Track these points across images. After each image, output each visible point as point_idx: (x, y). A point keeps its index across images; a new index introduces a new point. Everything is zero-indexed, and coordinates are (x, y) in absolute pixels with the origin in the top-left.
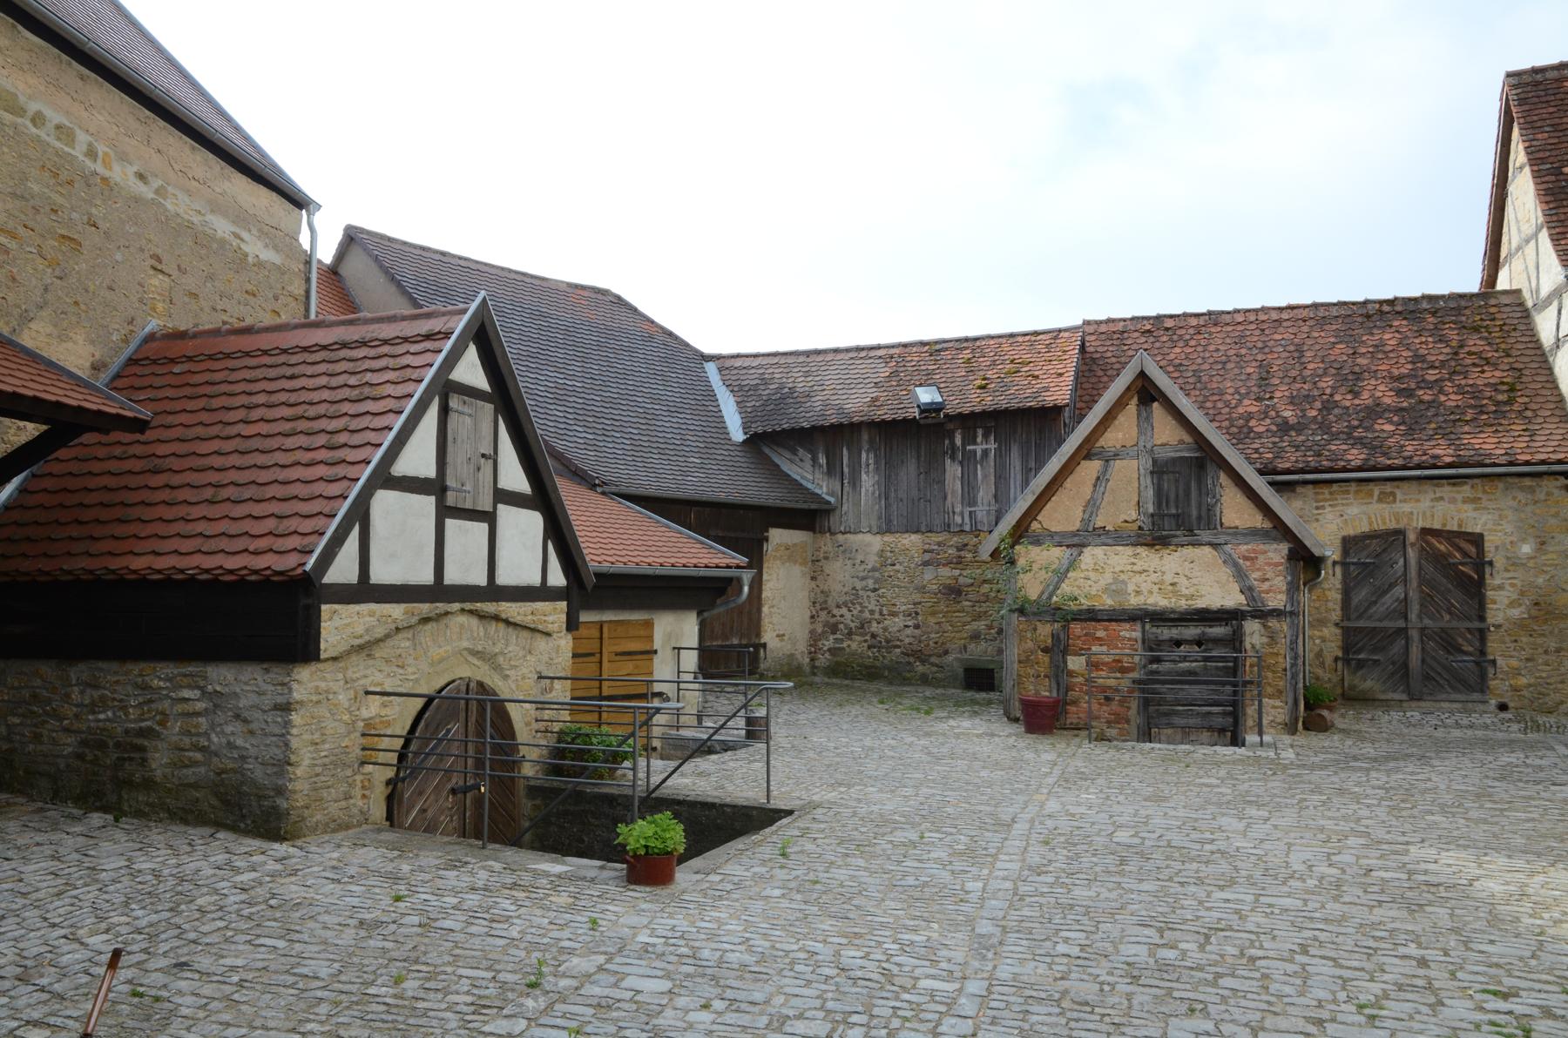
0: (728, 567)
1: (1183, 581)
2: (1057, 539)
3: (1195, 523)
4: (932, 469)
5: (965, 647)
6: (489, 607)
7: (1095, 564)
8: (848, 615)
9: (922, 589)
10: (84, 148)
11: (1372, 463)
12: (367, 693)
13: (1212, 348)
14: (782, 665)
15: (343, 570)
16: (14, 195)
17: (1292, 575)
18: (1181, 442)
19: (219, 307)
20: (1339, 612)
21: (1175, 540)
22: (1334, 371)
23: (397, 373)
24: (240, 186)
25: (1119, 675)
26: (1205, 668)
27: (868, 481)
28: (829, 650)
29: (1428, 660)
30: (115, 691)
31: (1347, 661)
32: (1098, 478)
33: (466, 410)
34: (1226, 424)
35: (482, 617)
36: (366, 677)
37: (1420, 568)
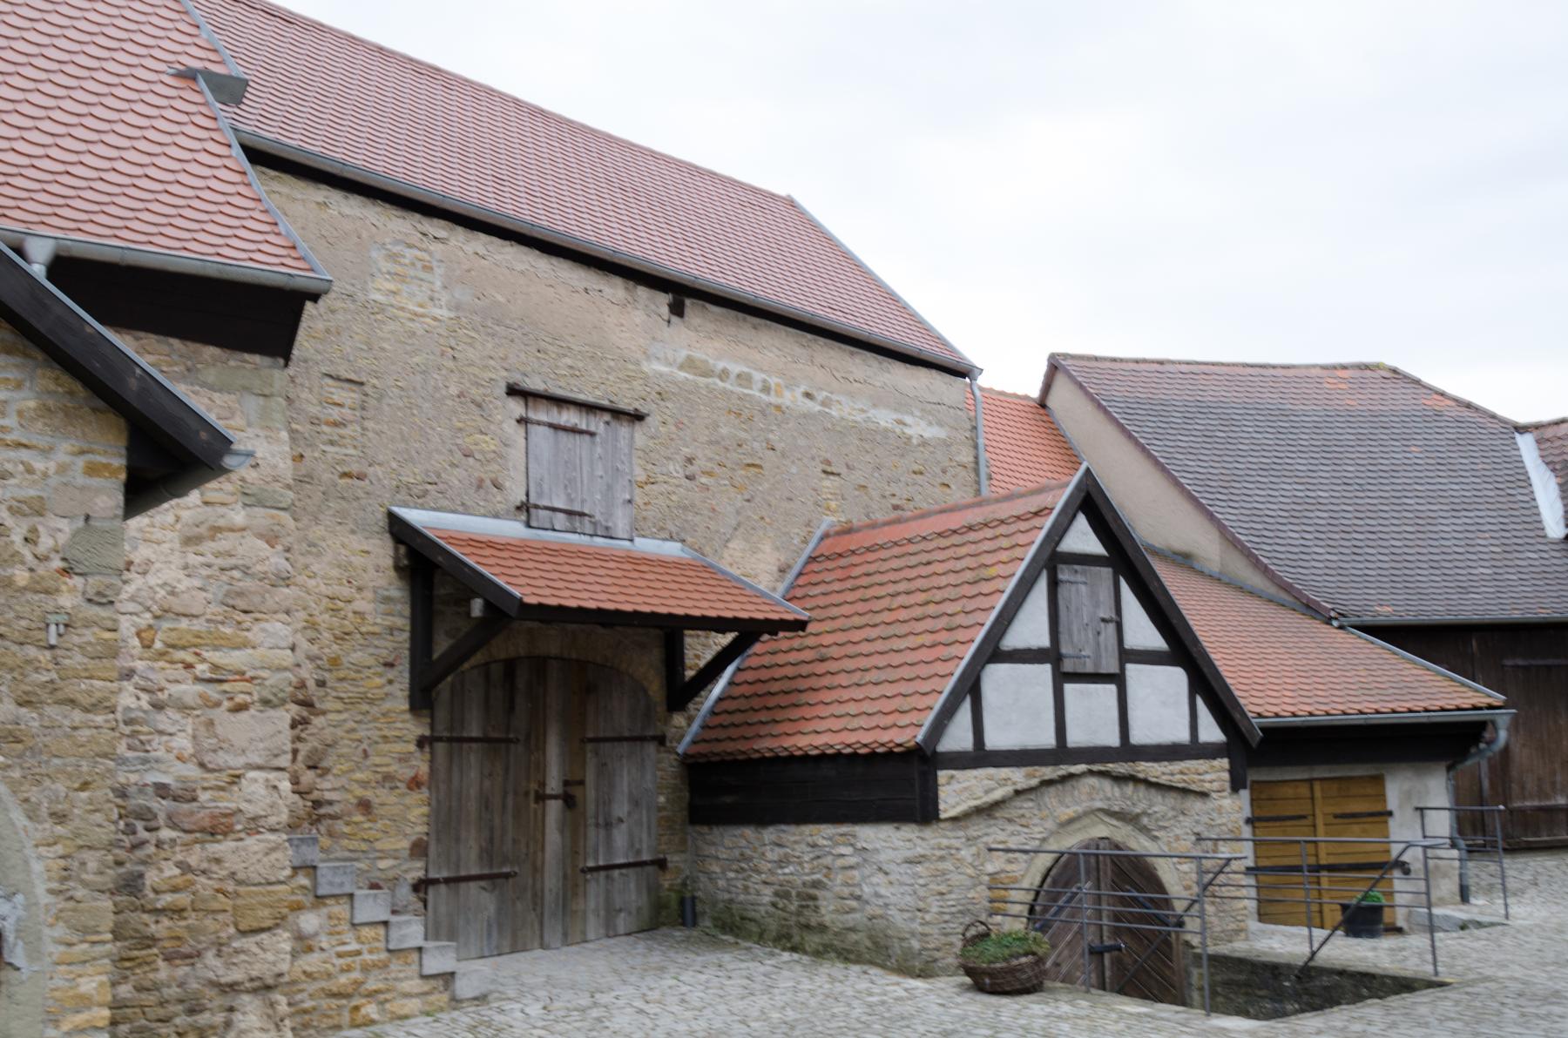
0: (1475, 708)
10: (760, 385)
12: (990, 850)
15: (958, 737)
16: (710, 443)
19: (887, 493)
24: (901, 375)
30: (793, 850)
33: (1079, 578)
35: (1119, 779)
36: (987, 834)
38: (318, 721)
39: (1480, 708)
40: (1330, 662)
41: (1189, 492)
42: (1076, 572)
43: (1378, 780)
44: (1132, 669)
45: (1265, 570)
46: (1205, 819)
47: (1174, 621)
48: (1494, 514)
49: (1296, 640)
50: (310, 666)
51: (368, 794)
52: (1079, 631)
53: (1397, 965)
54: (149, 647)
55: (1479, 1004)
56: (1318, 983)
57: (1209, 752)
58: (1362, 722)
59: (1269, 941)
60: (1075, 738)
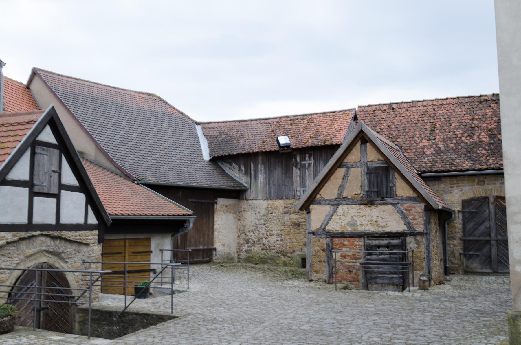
0: (184, 215)
1: (380, 220)
2: (328, 202)
3: (385, 194)
4: (288, 172)
5: (302, 249)
6: (55, 233)
7: (344, 213)
8: (253, 235)
9: (284, 224)
11: (473, 167)
13: (412, 117)
14: (224, 258)
17: (427, 217)
18: (379, 160)
20: (461, 233)
21: (377, 202)
22: (463, 127)
23: (13, 138)
25: (354, 261)
26: (390, 257)
27: (261, 177)
28: (246, 251)
29: (500, 254)
31: (465, 255)
32: (344, 176)
33: (45, 152)
34: (414, 150)
35: (54, 238)
37: (496, 213)
39: (185, 215)
40: (135, 196)
41: (85, 129)
42: (44, 149)
43: (148, 240)
44: (64, 194)
45: (112, 161)
46: (87, 254)
47: (83, 175)
48: (188, 150)
49: (123, 187)
52: (43, 175)
53: (156, 310)
54: (423, 268)
55: (191, 325)
56: (127, 318)
57: (91, 228)
58: (167, 219)
59: (107, 301)
60: (37, 220)
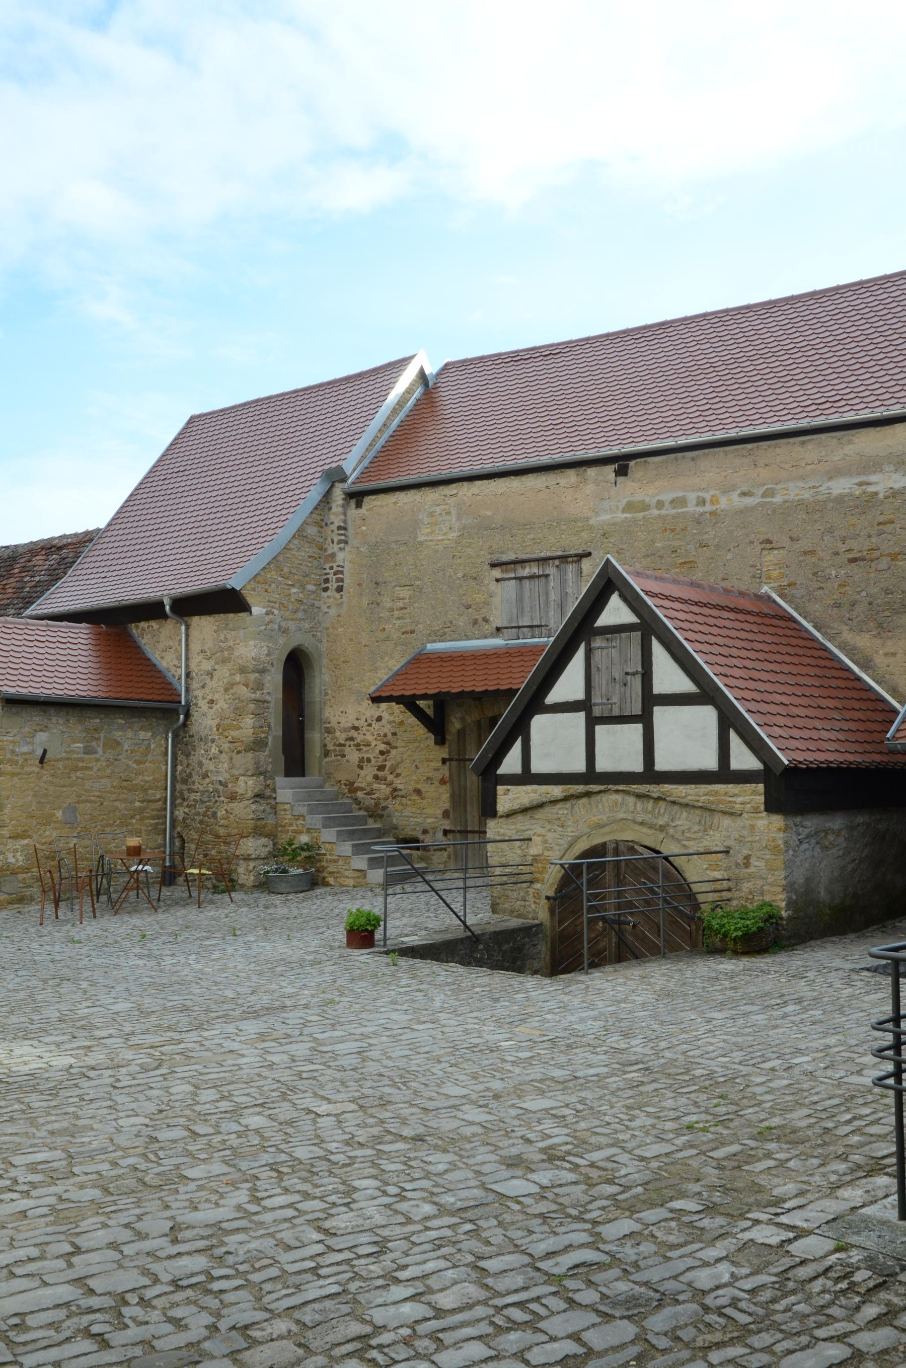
35: (639, 796)
38: (393, 752)
50: (389, 726)
51: (419, 786)
60: (661, 765)
